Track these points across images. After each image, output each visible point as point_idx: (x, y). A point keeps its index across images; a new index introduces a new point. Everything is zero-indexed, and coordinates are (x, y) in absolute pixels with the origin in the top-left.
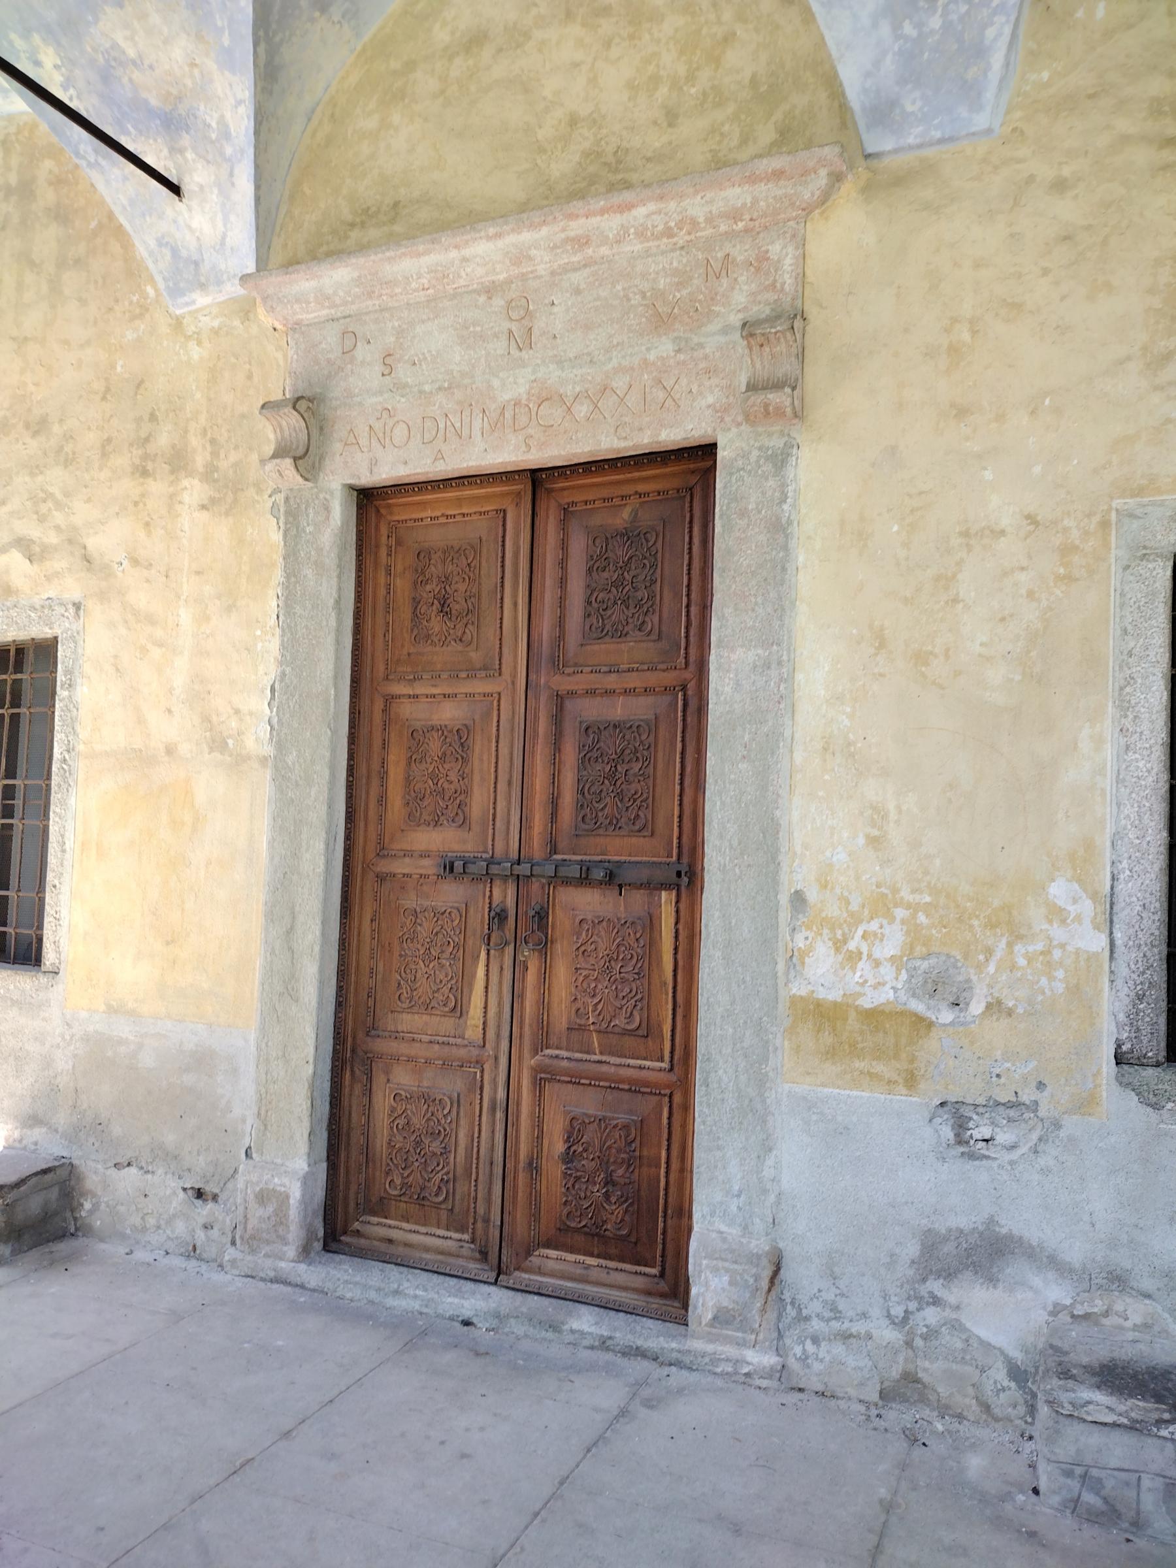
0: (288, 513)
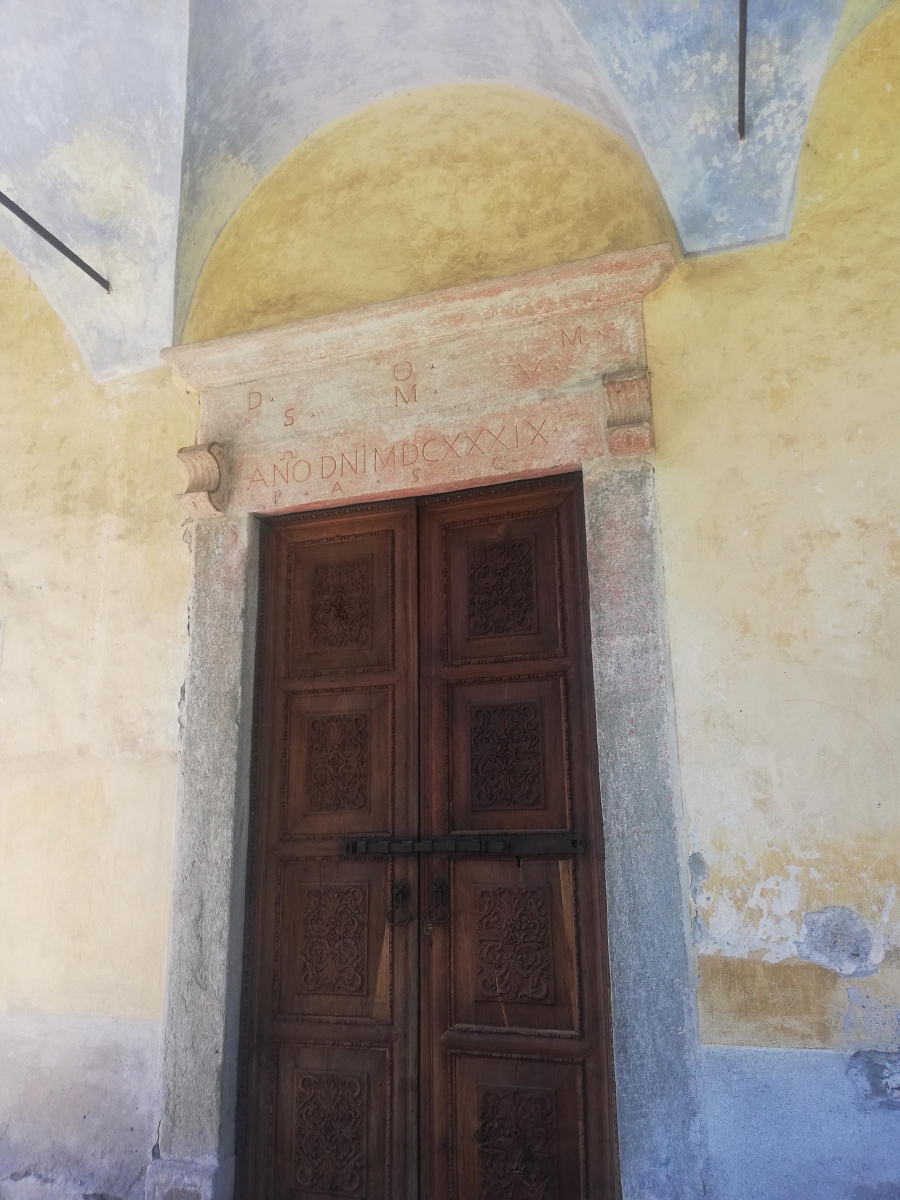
0: (199, 539)
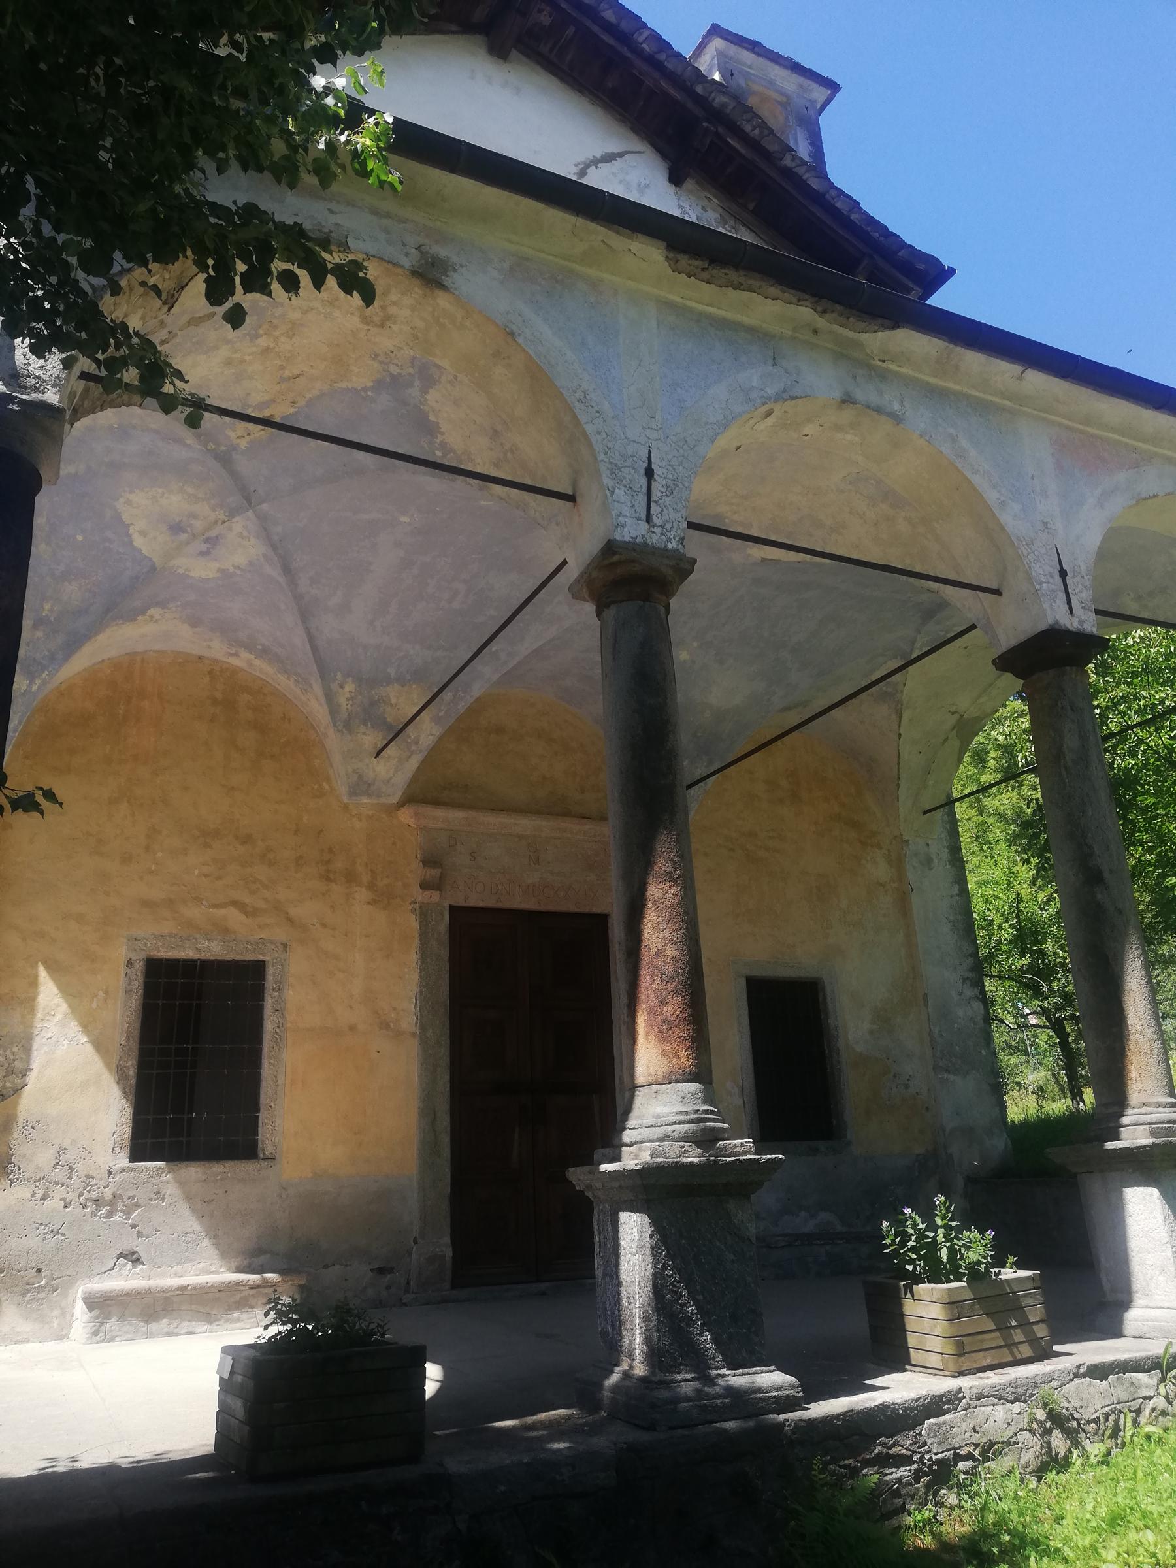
0: (422, 914)
